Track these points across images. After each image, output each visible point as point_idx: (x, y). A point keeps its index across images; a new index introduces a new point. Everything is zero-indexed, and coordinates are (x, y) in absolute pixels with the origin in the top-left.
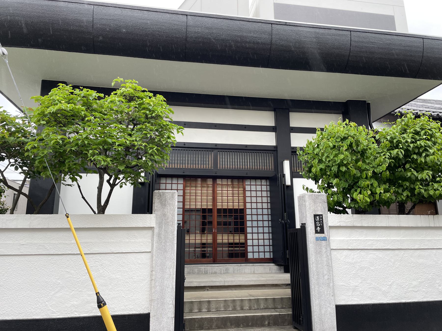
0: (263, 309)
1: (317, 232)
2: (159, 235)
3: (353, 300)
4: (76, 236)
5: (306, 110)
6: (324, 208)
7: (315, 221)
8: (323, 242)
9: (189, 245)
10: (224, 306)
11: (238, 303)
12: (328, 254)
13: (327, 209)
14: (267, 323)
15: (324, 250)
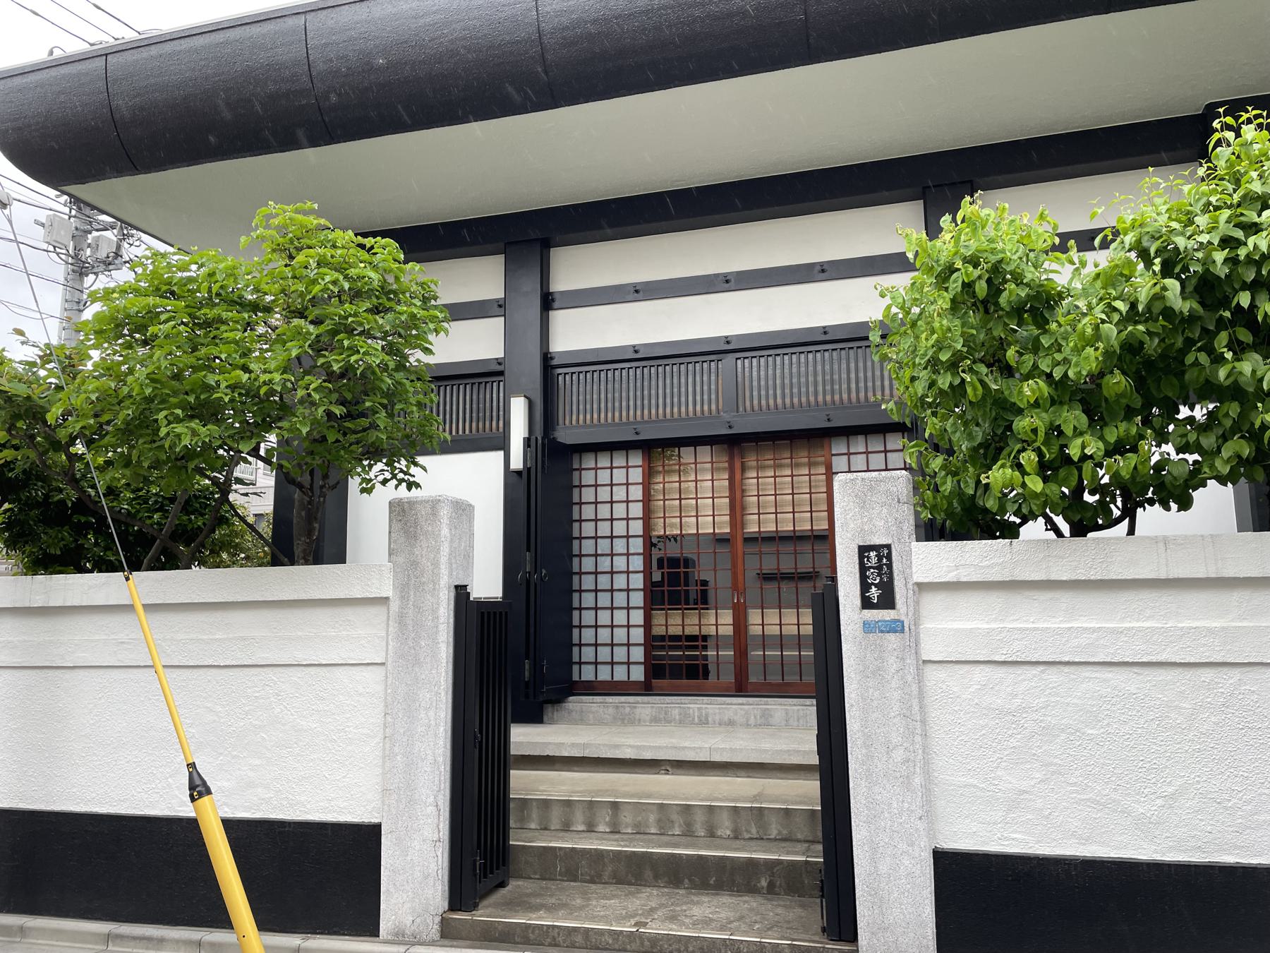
0: (776, 840)
1: (867, 604)
2: (401, 617)
3: (1006, 839)
4: (146, 626)
5: (1000, 178)
6: (899, 523)
7: (863, 569)
8: (892, 637)
9: (764, 641)
10: (659, 821)
11: (699, 818)
12: (910, 678)
13: (909, 526)
14: (764, 883)
15: (892, 664)
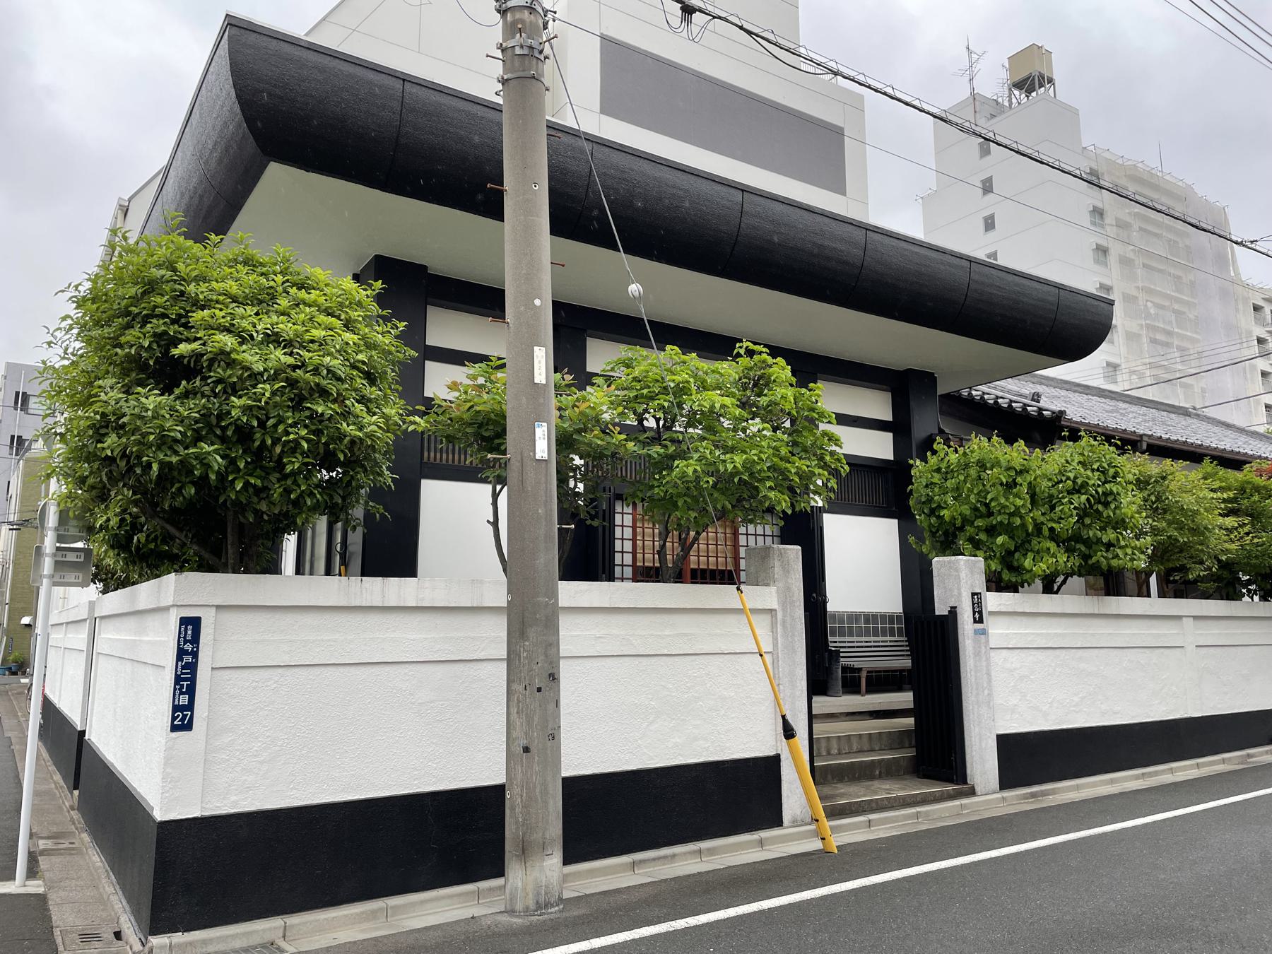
1: (975, 621)
